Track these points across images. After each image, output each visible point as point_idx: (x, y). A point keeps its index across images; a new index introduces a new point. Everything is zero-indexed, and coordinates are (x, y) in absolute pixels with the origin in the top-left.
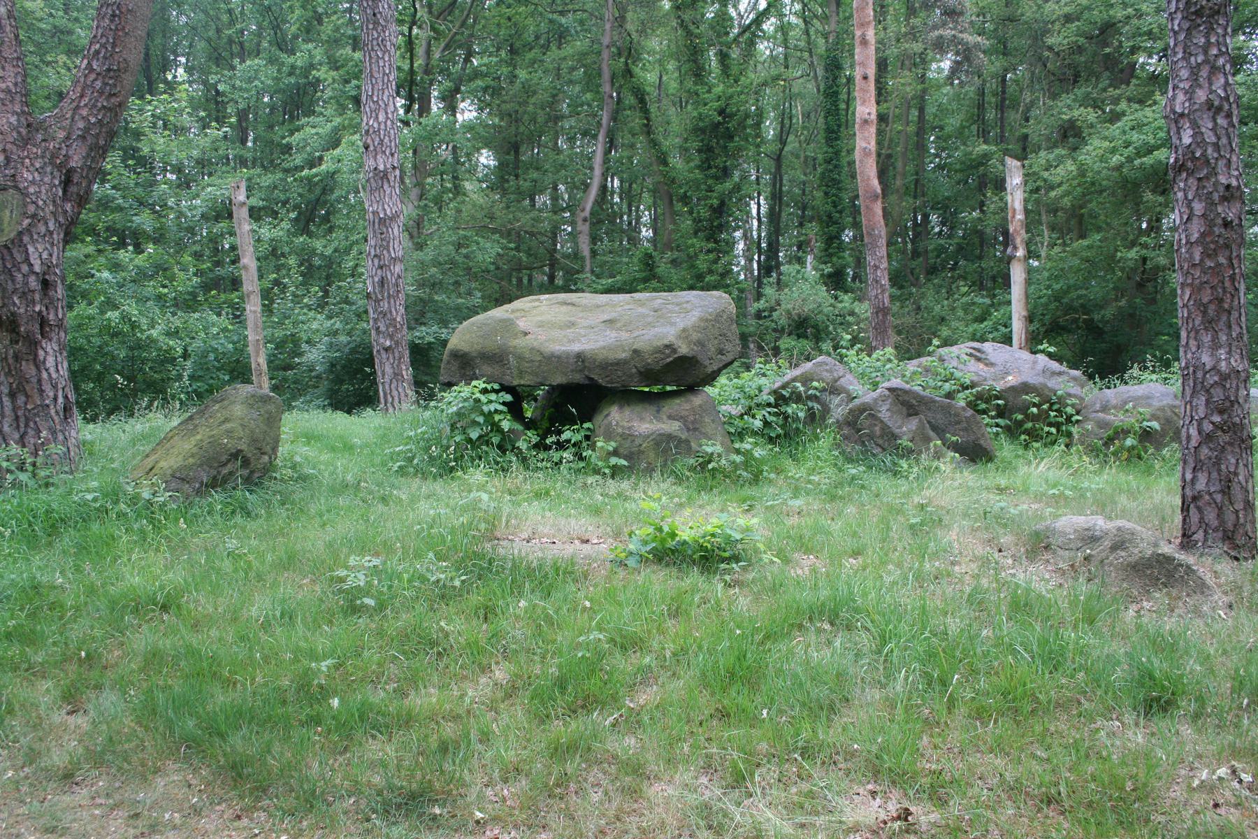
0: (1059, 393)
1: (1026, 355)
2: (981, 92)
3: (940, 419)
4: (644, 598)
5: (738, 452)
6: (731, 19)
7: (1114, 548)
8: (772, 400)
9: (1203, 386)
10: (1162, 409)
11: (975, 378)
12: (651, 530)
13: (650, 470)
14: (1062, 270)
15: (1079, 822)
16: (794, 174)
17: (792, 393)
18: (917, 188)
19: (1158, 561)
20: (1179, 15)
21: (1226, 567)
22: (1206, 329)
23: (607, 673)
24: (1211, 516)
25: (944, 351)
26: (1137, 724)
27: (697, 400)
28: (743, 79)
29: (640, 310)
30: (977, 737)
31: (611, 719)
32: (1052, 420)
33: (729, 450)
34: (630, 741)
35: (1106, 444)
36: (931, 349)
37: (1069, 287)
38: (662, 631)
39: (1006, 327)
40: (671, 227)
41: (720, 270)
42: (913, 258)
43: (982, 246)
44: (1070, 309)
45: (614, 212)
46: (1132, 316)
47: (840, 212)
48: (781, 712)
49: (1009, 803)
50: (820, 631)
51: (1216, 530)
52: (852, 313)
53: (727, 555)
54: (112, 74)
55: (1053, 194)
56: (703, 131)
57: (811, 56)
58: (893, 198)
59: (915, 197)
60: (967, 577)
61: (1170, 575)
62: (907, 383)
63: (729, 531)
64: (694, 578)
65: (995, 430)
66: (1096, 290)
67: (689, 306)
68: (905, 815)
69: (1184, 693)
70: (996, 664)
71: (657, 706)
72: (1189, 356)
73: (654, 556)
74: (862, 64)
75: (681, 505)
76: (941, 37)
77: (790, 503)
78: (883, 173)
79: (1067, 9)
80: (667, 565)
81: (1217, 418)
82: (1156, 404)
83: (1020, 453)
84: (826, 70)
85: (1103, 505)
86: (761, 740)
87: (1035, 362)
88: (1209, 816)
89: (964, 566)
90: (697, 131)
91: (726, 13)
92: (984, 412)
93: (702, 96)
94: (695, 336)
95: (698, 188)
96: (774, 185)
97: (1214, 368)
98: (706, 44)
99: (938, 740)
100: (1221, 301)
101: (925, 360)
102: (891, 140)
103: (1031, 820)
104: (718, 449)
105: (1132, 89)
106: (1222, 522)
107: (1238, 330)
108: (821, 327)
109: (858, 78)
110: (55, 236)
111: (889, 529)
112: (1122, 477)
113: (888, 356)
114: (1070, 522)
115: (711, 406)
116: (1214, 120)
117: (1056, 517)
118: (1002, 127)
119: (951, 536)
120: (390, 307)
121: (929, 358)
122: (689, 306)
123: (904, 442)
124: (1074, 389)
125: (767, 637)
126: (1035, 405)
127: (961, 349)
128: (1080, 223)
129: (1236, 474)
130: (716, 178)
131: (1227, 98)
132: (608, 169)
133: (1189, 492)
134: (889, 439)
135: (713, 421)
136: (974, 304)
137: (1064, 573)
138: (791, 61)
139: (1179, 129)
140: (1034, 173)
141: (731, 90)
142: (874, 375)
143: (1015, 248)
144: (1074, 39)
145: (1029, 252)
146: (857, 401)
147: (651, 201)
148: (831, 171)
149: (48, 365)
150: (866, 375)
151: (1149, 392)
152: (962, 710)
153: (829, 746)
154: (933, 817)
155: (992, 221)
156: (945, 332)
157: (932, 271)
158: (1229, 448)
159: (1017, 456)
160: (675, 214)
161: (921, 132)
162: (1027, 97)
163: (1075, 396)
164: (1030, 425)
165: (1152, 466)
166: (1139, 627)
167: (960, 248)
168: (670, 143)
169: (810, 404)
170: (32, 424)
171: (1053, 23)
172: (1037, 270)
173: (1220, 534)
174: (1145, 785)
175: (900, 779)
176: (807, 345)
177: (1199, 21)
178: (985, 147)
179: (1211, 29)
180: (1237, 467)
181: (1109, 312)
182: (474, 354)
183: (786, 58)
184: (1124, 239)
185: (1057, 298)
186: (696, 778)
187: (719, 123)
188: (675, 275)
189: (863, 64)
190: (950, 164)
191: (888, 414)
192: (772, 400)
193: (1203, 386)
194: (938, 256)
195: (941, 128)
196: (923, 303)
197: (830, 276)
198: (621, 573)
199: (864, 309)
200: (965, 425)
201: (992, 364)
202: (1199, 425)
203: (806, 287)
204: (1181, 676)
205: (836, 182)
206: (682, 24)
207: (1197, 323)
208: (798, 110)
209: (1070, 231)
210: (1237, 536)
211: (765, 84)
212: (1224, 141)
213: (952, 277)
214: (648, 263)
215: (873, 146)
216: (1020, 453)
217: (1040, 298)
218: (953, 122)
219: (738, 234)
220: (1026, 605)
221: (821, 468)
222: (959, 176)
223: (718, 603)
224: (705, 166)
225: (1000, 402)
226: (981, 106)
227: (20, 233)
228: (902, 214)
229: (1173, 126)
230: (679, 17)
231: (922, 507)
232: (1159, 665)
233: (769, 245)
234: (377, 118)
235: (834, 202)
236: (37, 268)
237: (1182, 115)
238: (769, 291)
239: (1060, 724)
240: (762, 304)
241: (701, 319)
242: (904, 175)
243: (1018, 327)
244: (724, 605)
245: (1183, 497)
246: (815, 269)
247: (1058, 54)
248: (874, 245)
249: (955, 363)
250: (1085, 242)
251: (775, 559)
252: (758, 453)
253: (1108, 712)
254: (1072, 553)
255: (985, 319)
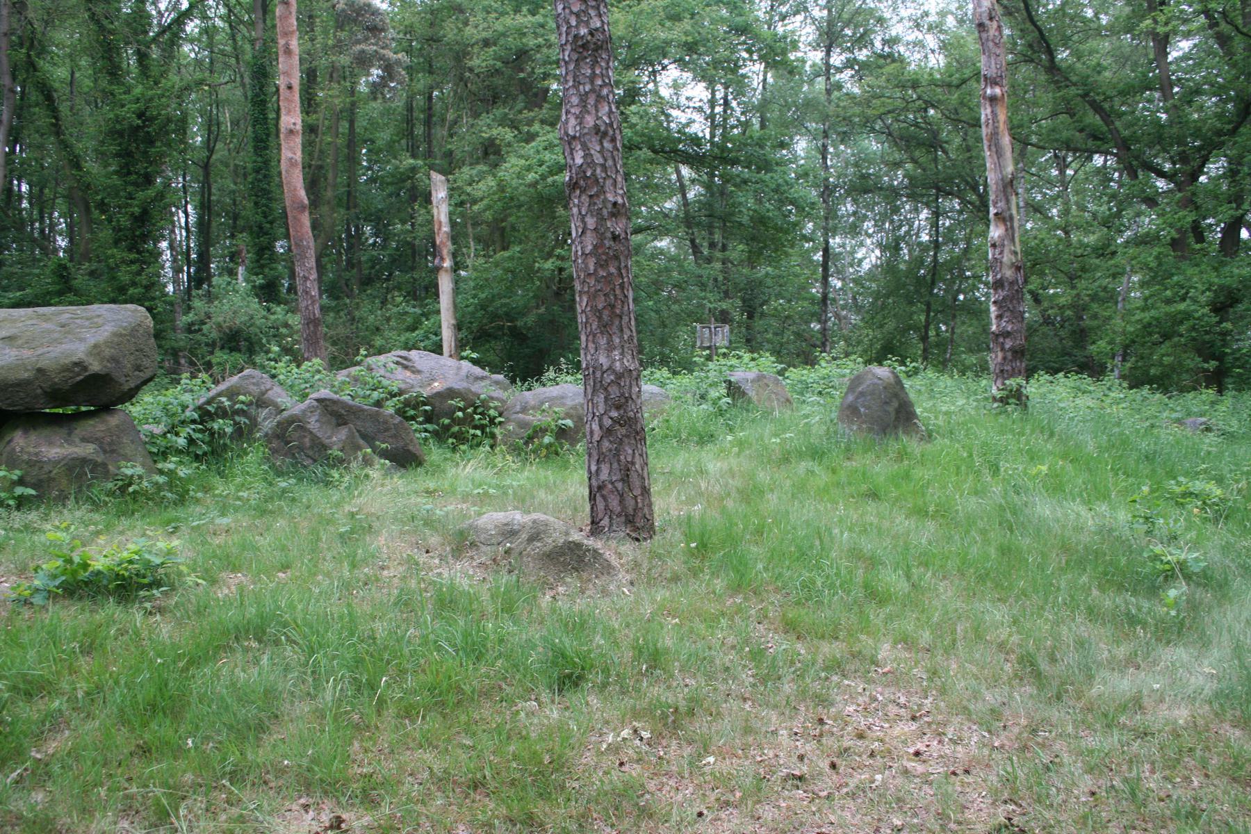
0: (482, 396)
1: (452, 362)
2: (410, 108)
3: (370, 428)
4: (53, 637)
5: (161, 472)
6: (150, 16)
7: (531, 539)
8: (196, 416)
9: (602, 385)
10: (574, 408)
11: (403, 386)
12: (59, 563)
13: (62, 499)
14: (487, 280)
15: (502, 800)
16: (224, 184)
17: (219, 407)
18: (349, 199)
19: (569, 549)
20: (569, 47)
21: (628, 548)
22: (602, 333)
23: (9, 724)
24: (614, 503)
25: (371, 360)
26: (553, 702)
27: (113, 421)
28: (163, 81)
29: (45, 325)
30: (407, 735)
31: (14, 775)
32: (477, 423)
33: (151, 471)
34: (39, 796)
35: (526, 443)
36: (359, 358)
37: (493, 296)
38: (73, 671)
39: (436, 335)
40: (88, 236)
41: (144, 282)
42: (346, 269)
43: (414, 257)
44: (495, 317)
45: (22, 219)
46: (552, 322)
47: (271, 223)
48: (207, 738)
49: (439, 794)
50: (247, 650)
51: (619, 515)
52: (286, 325)
53: (146, 581)
55: (476, 208)
56: (121, 134)
57: (238, 63)
58: (325, 209)
59: (348, 209)
60: (396, 580)
61: (581, 560)
62: (336, 393)
63: (147, 556)
64: (111, 609)
65: (423, 435)
66: (520, 296)
67: (100, 321)
68: (337, 823)
69: (592, 666)
70: (422, 661)
71: (69, 754)
72: (589, 357)
73: (65, 589)
74: (286, 73)
75: (98, 533)
76: (363, 51)
77: (218, 521)
78: (312, 185)
79: (484, 34)
80: (81, 598)
81: (614, 414)
82: (569, 403)
83: (448, 456)
84: (253, 78)
85: (523, 500)
86: (185, 772)
87: (459, 368)
88: (615, 775)
89: (392, 570)
90: (115, 133)
91: (144, 11)
92: (413, 418)
93: (119, 97)
94: (108, 352)
95: (117, 195)
96: (203, 196)
97: (610, 368)
98: (120, 41)
99: (368, 744)
100: (613, 307)
101: (354, 370)
102: (321, 151)
103: (460, 806)
104: (139, 470)
105: (545, 112)
106: (624, 507)
107: (629, 333)
108: (254, 339)
109: (282, 88)
111: (319, 539)
112: (542, 473)
113: (316, 367)
114: (492, 518)
115: (130, 427)
116: (601, 144)
117: (480, 514)
118: (430, 143)
119: (381, 542)
121: (358, 368)
122: (100, 321)
123: (335, 452)
124: (498, 393)
125: (191, 662)
126: (460, 409)
127: (388, 358)
128: (502, 235)
129: (633, 463)
130: (135, 184)
131: (611, 125)
132: (12, 171)
133: (594, 483)
134: (319, 450)
135: (133, 442)
136: (406, 313)
137: (487, 567)
138: (218, 66)
139: (572, 150)
140: (459, 188)
141: (150, 93)
142: (303, 386)
143: (442, 259)
144: (492, 62)
145: (456, 264)
146: (285, 414)
147: (64, 208)
148: (260, 181)
150: (294, 386)
151: (561, 393)
152: (391, 711)
153: (258, 766)
154: (366, 820)
155: (421, 233)
156: (378, 342)
157: (367, 282)
158: (626, 440)
159: (446, 459)
160: (91, 221)
161: (352, 143)
162: (451, 116)
163: (497, 399)
164: (456, 429)
165: (568, 461)
166: (553, 611)
167: (393, 261)
168: (85, 146)
169: (237, 418)
171: (472, 46)
172: (465, 280)
173: (623, 519)
174: (560, 757)
175: (332, 788)
176: (239, 358)
177: (585, 54)
178: (412, 161)
179: (595, 62)
180: (633, 457)
181: (530, 319)
183: (212, 62)
184: (541, 251)
185: (483, 306)
186: (115, 823)
187: (138, 126)
188: (93, 287)
189: (288, 74)
190: (382, 177)
191: (318, 425)
192: (196, 416)
193: (602, 385)
194: (373, 267)
195: (373, 142)
196: (357, 314)
197: (262, 287)
198: (26, 613)
199: (295, 320)
200: (393, 432)
201: (419, 372)
202: (600, 420)
203: (237, 299)
204: (589, 651)
205: (266, 192)
206: (93, 16)
207: (594, 327)
208: (226, 117)
209: (494, 243)
210: (638, 519)
211: (187, 88)
212: (610, 162)
213: (387, 288)
214: (63, 274)
215: (299, 156)
216: (448, 456)
217: (467, 306)
218: (383, 137)
219: (164, 245)
220: (451, 602)
221: (251, 483)
222: (390, 189)
223: (137, 633)
224: (125, 171)
225: (427, 408)
226: (409, 121)
228: (334, 225)
229: (567, 147)
230: (90, 9)
231: (352, 515)
232: (568, 643)
233: (200, 255)
235: (264, 212)
237: (574, 137)
238: (197, 303)
239: (485, 711)
240: (190, 317)
241: (114, 334)
242: (335, 186)
243: (448, 336)
244: (145, 634)
245: (590, 487)
246: (247, 281)
247: (478, 75)
248: (303, 256)
249: (382, 372)
250: (506, 254)
251: (200, 581)
252: (183, 472)
253: (527, 694)
254: (494, 548)
255: (416, 328)
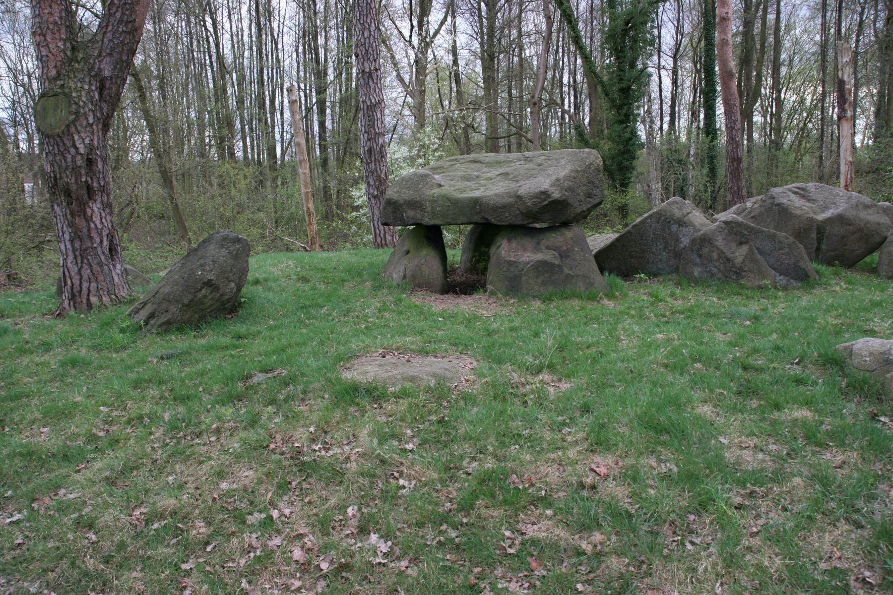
54: (128, 6)
110: (95, 127)
120: (376, 168)
149: (94, 219)
170: (85, 261)
182: (402, 202)
200: (787, 250)
227: (68, 126)
234: (363, 34)
236: (82, 151)
241: (572, 171)
